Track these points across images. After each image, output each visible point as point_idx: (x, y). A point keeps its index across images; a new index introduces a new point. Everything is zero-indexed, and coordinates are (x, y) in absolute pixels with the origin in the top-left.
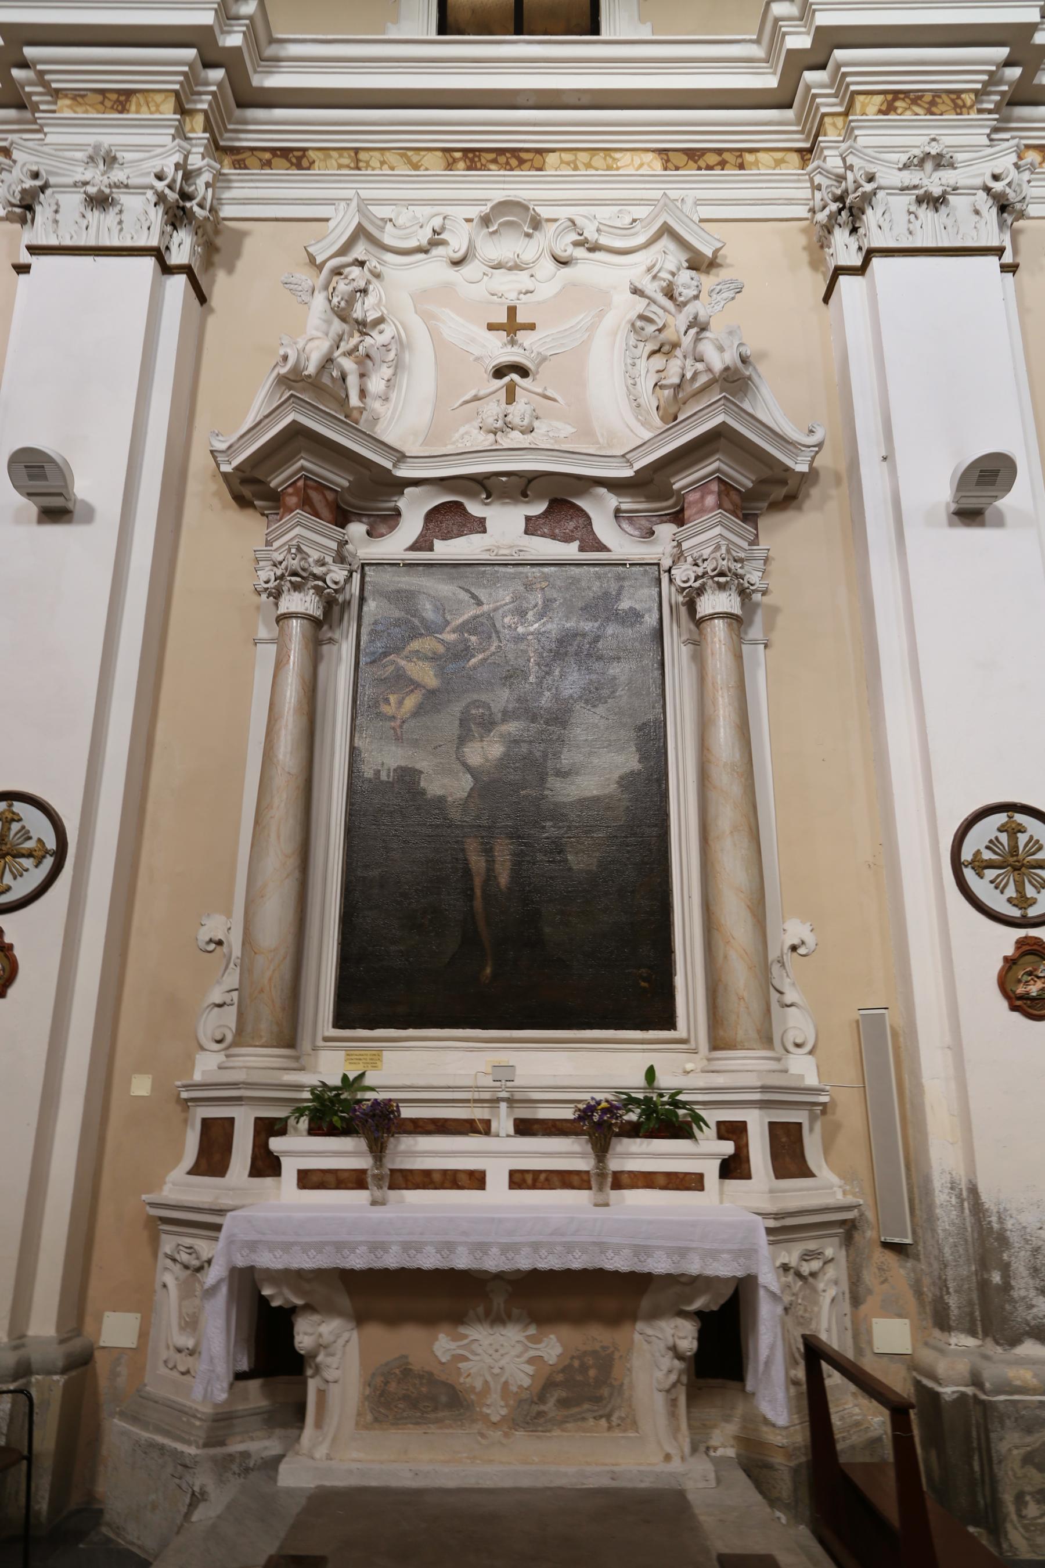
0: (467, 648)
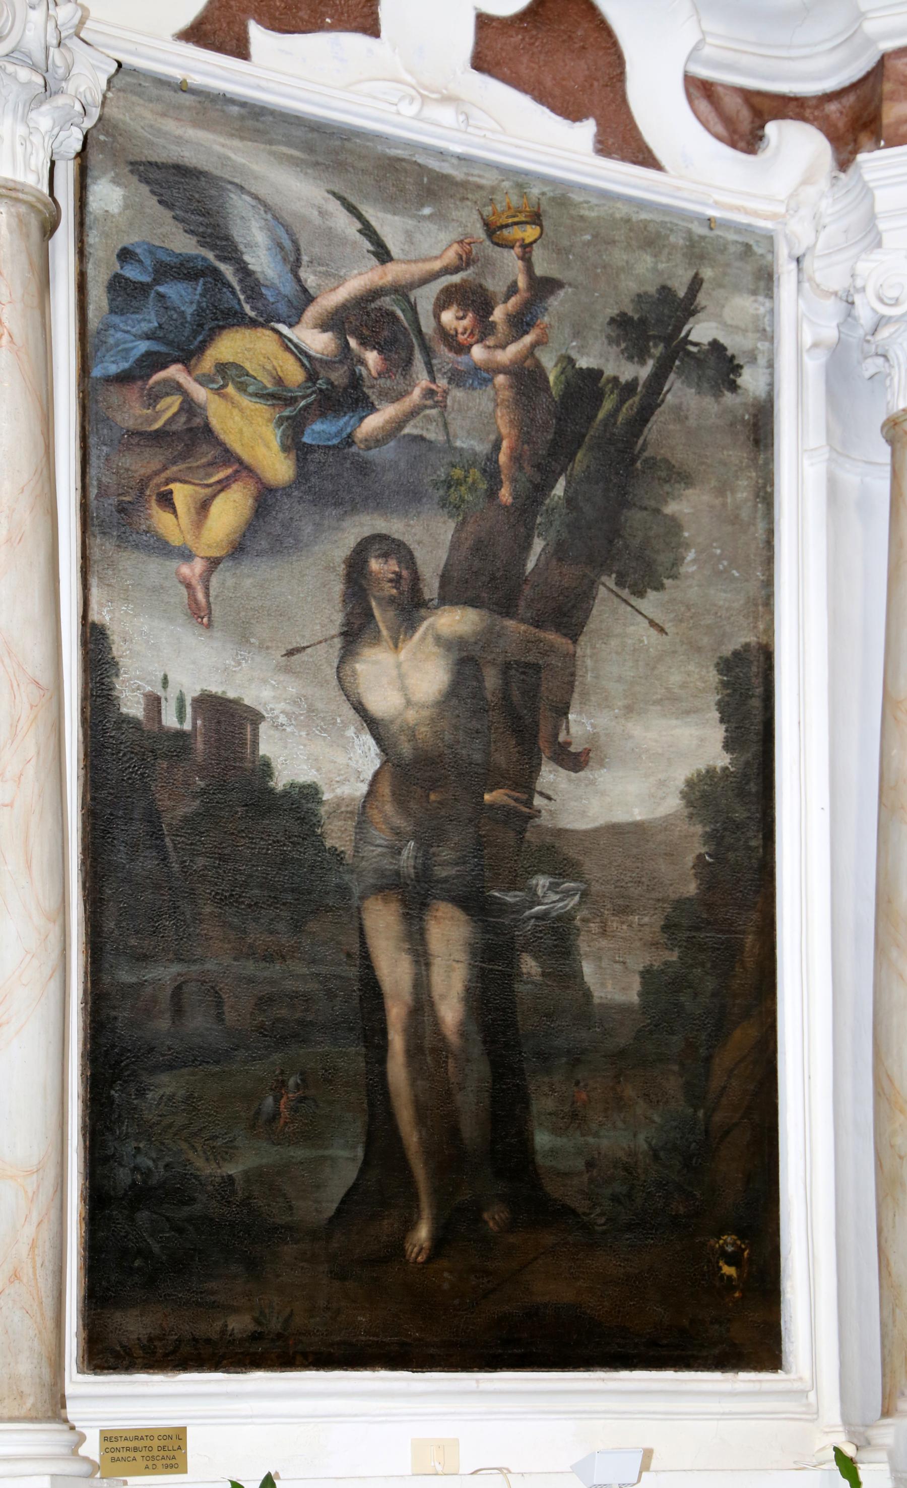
0: (356, 381)
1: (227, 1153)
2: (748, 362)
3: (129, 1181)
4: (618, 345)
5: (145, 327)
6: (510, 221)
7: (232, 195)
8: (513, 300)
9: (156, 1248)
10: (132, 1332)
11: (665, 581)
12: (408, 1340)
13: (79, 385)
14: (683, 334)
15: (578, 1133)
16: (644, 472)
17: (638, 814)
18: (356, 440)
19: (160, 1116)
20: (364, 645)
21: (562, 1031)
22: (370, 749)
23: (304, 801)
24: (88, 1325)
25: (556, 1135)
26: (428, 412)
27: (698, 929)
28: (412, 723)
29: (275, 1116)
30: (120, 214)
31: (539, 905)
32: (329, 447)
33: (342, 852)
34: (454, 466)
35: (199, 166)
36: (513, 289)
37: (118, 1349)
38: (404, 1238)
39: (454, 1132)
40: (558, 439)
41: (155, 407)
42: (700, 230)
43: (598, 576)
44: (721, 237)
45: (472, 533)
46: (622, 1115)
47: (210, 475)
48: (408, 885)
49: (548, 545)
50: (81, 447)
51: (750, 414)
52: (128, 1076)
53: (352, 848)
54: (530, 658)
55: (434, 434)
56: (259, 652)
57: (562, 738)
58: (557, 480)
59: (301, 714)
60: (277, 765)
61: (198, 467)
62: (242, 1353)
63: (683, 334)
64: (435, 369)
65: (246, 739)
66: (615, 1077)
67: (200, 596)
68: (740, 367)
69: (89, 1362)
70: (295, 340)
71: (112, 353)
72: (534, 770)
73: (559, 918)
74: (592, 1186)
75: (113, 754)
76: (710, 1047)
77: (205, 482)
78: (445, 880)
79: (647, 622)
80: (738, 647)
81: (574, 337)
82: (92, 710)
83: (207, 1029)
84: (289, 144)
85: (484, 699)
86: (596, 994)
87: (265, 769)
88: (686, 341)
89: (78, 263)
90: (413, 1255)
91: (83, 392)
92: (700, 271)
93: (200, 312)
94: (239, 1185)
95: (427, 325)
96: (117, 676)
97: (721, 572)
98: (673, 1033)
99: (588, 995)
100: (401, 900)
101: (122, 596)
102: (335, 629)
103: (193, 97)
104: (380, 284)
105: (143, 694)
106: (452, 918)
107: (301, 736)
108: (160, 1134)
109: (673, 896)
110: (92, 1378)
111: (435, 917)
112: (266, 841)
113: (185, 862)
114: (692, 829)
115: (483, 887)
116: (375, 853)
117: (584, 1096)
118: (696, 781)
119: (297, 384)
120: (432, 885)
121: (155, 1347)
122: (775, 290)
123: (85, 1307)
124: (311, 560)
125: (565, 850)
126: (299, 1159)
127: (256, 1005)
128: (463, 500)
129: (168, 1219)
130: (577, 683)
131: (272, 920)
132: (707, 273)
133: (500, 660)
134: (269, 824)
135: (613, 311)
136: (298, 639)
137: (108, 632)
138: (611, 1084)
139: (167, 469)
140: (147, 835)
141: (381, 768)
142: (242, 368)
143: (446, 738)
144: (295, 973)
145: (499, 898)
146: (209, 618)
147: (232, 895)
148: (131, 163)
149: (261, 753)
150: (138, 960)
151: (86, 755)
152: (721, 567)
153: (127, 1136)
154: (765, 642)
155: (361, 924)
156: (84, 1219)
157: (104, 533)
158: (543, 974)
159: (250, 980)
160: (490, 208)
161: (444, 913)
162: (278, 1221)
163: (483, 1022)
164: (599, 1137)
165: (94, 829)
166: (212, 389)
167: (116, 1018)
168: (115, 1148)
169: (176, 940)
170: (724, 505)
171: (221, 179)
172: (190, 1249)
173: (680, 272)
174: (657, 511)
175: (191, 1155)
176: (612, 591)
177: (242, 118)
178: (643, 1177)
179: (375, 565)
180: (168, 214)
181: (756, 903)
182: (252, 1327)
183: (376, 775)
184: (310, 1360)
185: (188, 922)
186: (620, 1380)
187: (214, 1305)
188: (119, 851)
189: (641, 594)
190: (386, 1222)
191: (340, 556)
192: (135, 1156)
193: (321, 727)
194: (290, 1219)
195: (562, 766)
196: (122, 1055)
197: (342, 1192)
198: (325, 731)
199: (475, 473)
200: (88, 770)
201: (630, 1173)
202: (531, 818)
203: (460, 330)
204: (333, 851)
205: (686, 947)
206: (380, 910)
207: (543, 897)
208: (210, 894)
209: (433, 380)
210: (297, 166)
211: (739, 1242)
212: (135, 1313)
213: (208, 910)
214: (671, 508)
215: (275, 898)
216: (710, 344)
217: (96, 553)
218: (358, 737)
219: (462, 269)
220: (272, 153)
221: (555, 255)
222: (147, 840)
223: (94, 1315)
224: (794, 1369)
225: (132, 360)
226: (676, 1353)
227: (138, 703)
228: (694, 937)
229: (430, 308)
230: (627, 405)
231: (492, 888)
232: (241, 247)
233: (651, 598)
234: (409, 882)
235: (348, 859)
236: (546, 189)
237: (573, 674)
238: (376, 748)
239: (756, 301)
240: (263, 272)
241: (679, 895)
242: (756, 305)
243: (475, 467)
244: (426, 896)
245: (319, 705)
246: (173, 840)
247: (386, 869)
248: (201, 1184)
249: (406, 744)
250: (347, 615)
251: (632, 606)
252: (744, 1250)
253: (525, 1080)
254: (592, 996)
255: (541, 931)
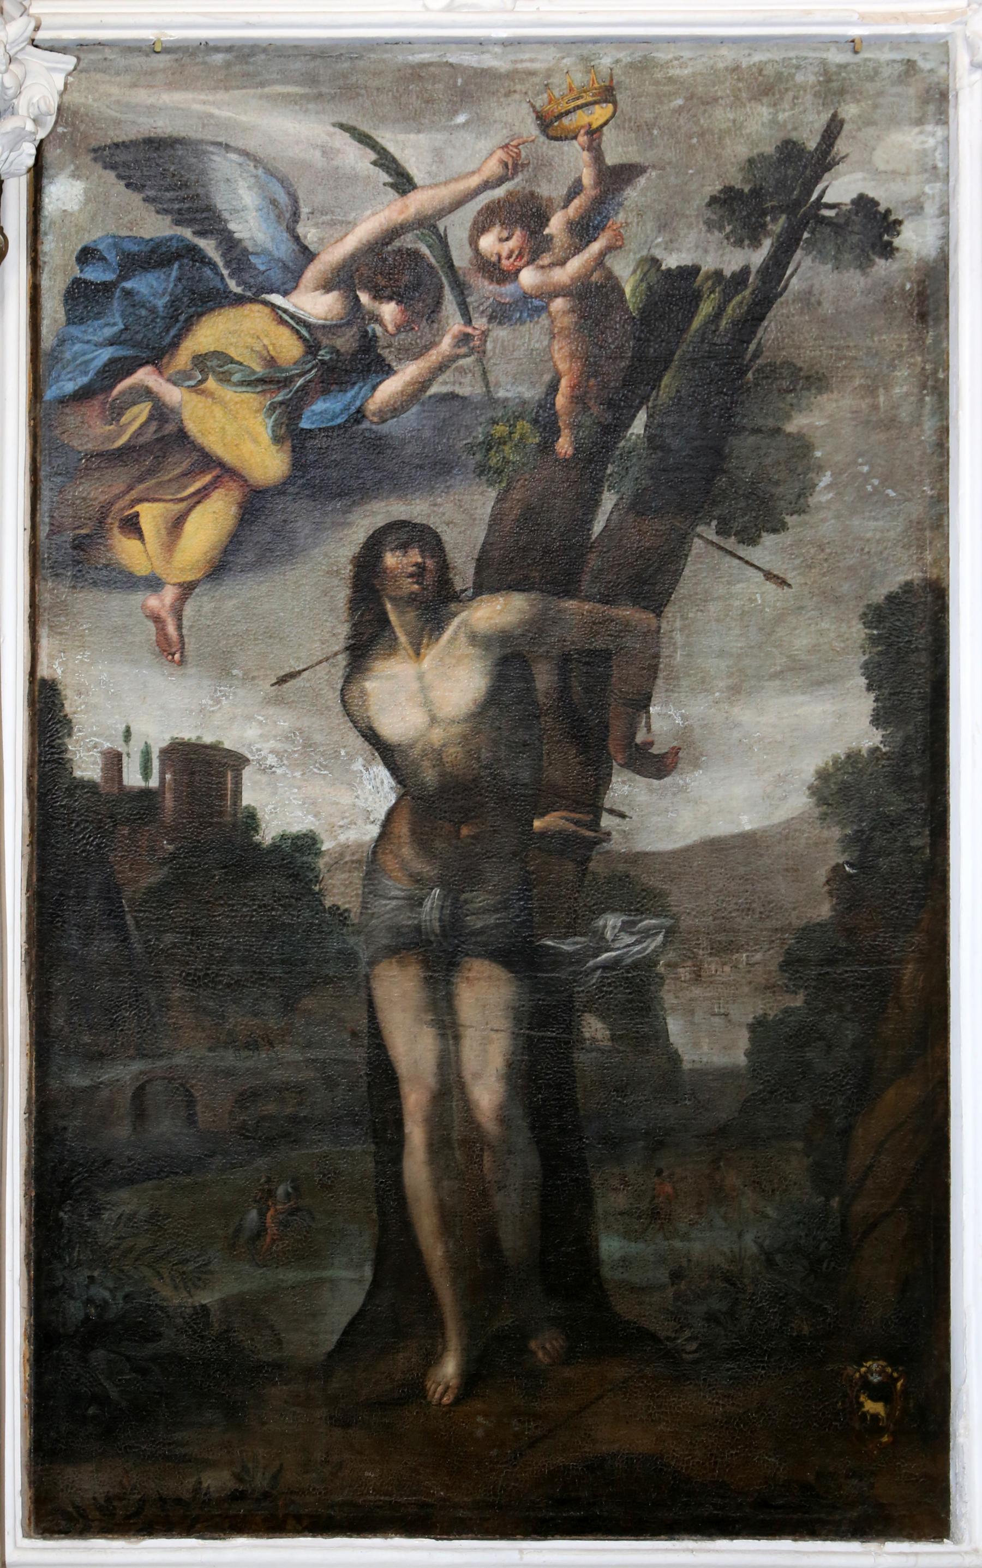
0: (368, 343)
1: (199, 1279)
2: (911, 214)
3: (81, 1316)
4: (721, 229)
5: (108, 332)
6: (573, 105)
7: (215, 158)
8: (576, 202)
9: (114, 1393)
10: (86, 1490)
11: (788, 519)
12: (429, 1500)
13: (30, 412)
14: (814, 196)
15: (660, 1235)
16: (757, 385)
17: (747, 823)
18: (368, 414)
19: (119, 1239)
20: (376, 659)
21: (639, 1108)
22: (382, 783)
23: (297, 855)
24: (34, 1483)
25: (630, 1240)
26: (462, 362)
27: (831, 962)
28: (437, 745)
29: (260, 1233)
30: (81, 210)
31: (607, 951)
32: (333, 428)
33: (346, 910)
34: (494, 422)
35: (175, 134)
36: (576, 189)
37: (71, 1509)
38: (425, 1375)
39: (492, 1244)
40: (637, 364)
41: (119, 421)
42: (836, 57)
43: (693, 526)
44: (869, 60)
45: (519, 501)
46: (723, 1210)
47: (185, 487)
48: (431, 942)
49: (622, 498)
50: (31, 482)
51: (912, 282)
52: (81, 1194)
53: (358, 904)
54: (599, 644)
55: (469, 388)
56: (243, 684)
57: (640, 738)
58: (634, 416)
59: (295, 752)
60: (264, 816)
61: (170, 480)
62: (220, 1515)
63: (814, 196)
64: (471, 309)
65: (226, 789)
66: (713, 1162)
67: (171, 629)
68: (899, 222)
69: (37, 1525)
70: (292, 309)
71: (68, 370)
72: (602, 782)
73: (635, 966)
74: (679, 1303)
75: (64, 826)
76: (850, 1115)
77: (179, 496)
78: (481, 932)
79: (761, 574)
80: (894, 588)
81: (659, 231)
82: (40, 777)
83: (176, 1134)
84: (285, 81)
85: (535, 703)
86: (686, 1058)
87: (249, 821)
88: (819, 204)
89: (30, 275)
90: (437, 1396)
91: (34, 419)
92: (839, 110)
93: (174, 303)
94: (215, 1317)
95: (461, 257)
96: (70, 735)
97: (871, 494)
98: (796, 1100)
99: (674, 1058)
100: (422, 961)
101: (77, 643)
102: (339, 643)
103: (167, 57)
104: (399, 221)
105: (100, 752)
106: (490, 977)
107: (294, 777)
108: (119, 1259)
109: (797, 923)
110: (40, 1543)
111: (467, 978)
112: (250, 906)
113: (150, 940)
114: (826, 834)
115: (532, 936)
116: (388, 908)
117: (668, 1188)
118: (831, 770)
119: (292, 361)
120: (463, 939)
121: (115, 1508)
122: (951, 111)
123: (30, 1461)
124: (308, 567)
125: (644, 878)
126: (290, 1283)
127: (236, 1102)
128: (506, 461)
129: (128, 1359)
130: (661, 666)
131: (257, 1000)
132: (849, 111)
133: (555, 652)
134: (253, 887)
135: (714, 187)
136: (292, 662)
137: (60, 687)
138: (707, 1172)
139: (132, 489)
140: (104, 914)
141: (396, 804)
142: (226, 355)
143: (483, 757)
144: (284, 1060)
145: (553, 948)
146: (182, 653)
147: (207, 975)
148: (95, 150)
149: (245, 803)
150: (92, 1059)
151: (32, 830)
152: (869, 488)
153: (79, 1263)
154: (935, 576)
155: (370, 995)
156: (28, 1360)
157: (57, 575)
158: (613, 1038)
159: (229, 1073)
160: (545, 96)
161: (478, 972)
162: (262, 1357)
163: (531, 1103)
164: (689, 1240)
165: (40, 914)
166: (189, 387)
167: (65, 1129)
168: (65, 1279)
169: (138, 1032)
170: (875, 407)
171: (201, 142)
172: (155, 1393)
173: (811, 117)
174: (778, 430)
175: (156, 1283)
176: (712, 543)
177: (228, 65)
178: (750, 1289)
179: (391, 560)
180: (135, 198)
181: (918, 922)
182: (232, 1484)
183: (391, 814)
184: (305, 1524)
185: (153, 1010)
186: (717, 1551)
187: (185, 1459)
188: (70, 936)
189: (753, 541)
190: (401, 1355)
191: (347, 556)
192: (87, 1287)
193: (320, 763)
194: (278, 1354)
195: (639, 773)
196: (73, 1170)
197: (345, 1320)
198: (325, 767)
199: (524, 426)
200: (35, 847)
201: (734, 1285)
202: (596, 843)
203: (504, 254)
204: (335, 909)
205: (814, 987)
206: (394, 976)
207: (613, 940)
208: (180, 975)
209: (469, 322)
210: (296, 103)
211: (889, 1370)
212: (91, 1469)
213: (177, 994)
214: (797, 424)
215: (260, 973)
216: (854, 202)
217: (46, 599)
218: (367, 770)
219: (508, 180)
220: (268, 97)
221: (633, 135)
222: (104, 920)
223: (42, 1470)
224: (966, 1537)
225: (91, 374)
226: (795, 1517)
227: (94, 763)
228: (827, 973)
229: (465, 235)
230: (734, 302)
231: (544, 936)
232: (226, 215)
233: (767, 543)
234: (432, 938)
235: (354, 918)
236: (621, 55)
237: (656, 656)
238: (391, 780)
239: (921, 133)
240: (252, 238)
241: (805, 921)
242: (922, 138)
243: (523, 419)
244: (454, 954)
245: (318, 738)
246: (135, 918)
247: (403, 926)
248: (168, 1316)
249: (430, 771)
250: (354, 625)
251: (740, 558)
252: (897, 1380)
253: (587, 1172)
254: (681, 1061)
255: (609, 984)
